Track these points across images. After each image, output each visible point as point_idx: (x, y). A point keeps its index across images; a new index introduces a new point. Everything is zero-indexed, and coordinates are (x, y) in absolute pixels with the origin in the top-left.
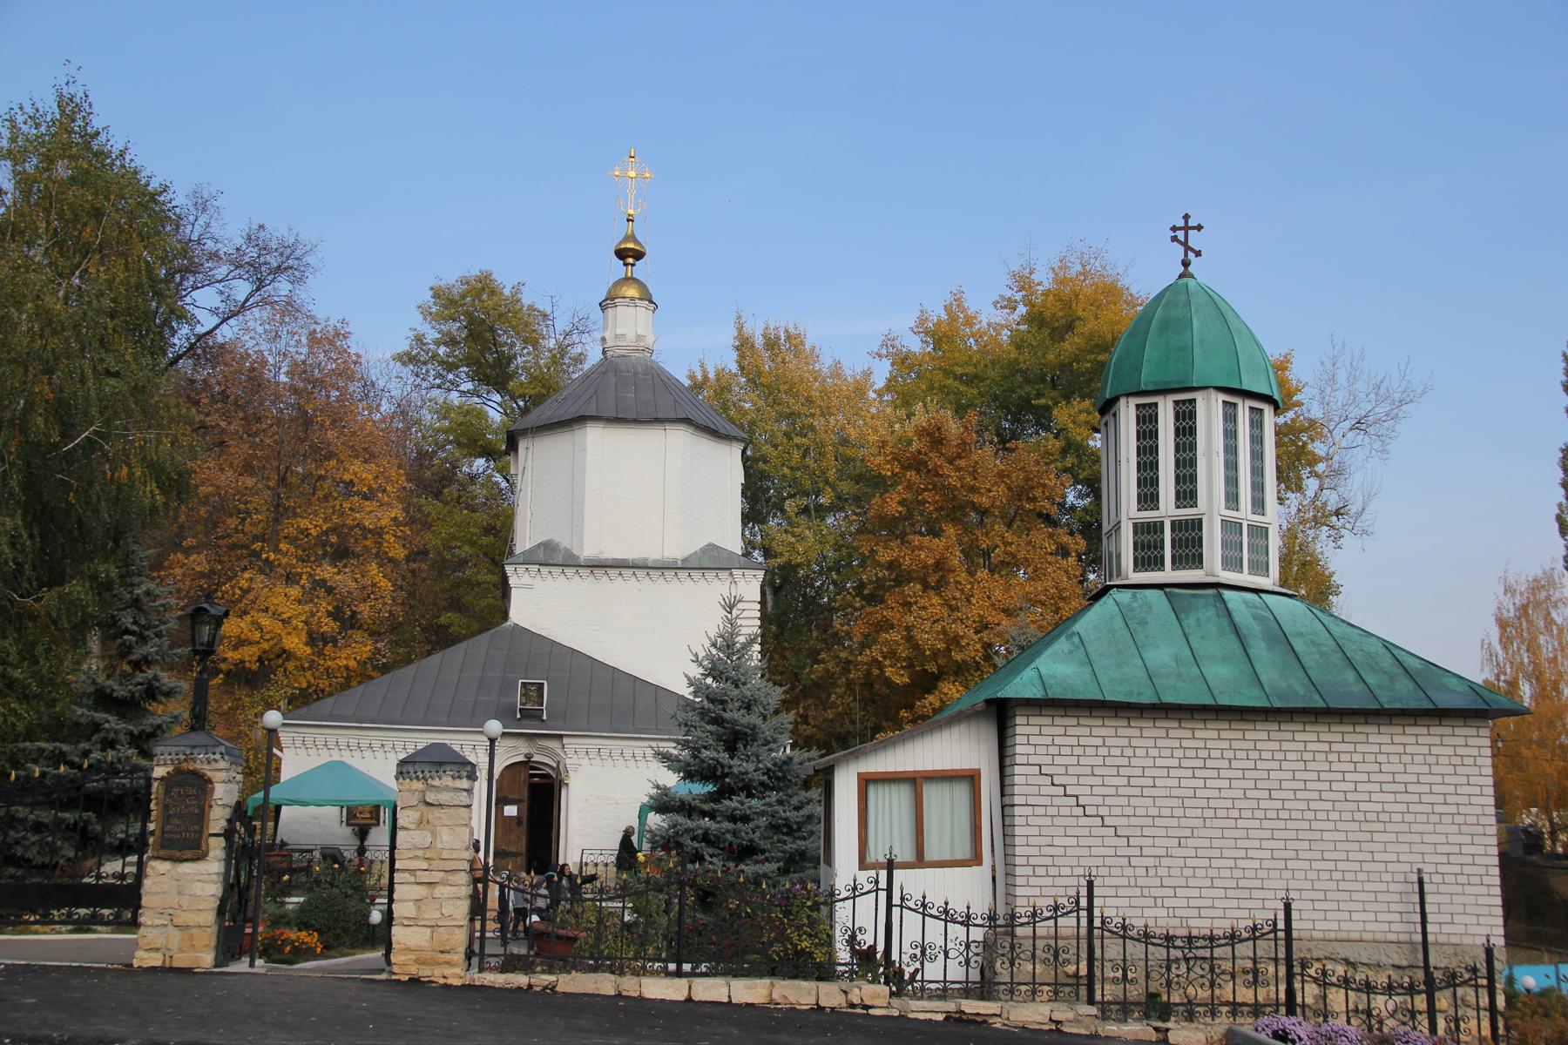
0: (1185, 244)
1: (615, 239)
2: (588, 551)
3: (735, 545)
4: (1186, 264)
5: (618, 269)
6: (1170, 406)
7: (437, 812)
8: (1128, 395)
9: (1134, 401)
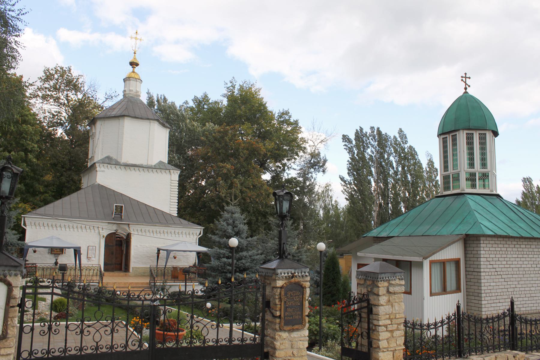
0: (465, 82)
1: (131, 59)
2: (123, 160)
3: (166, 160)
4: (466, 89)
5: (130, 68)
6: (478, 135)
7: (394, 297)
8: (463, 129)
9: (465, 132)
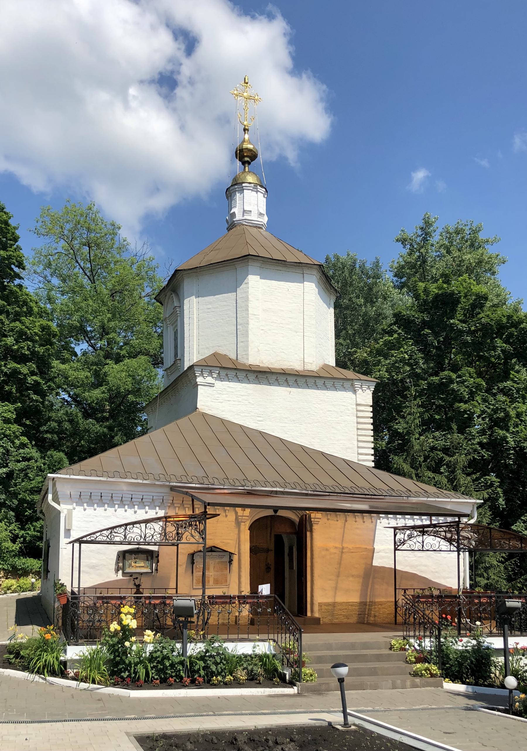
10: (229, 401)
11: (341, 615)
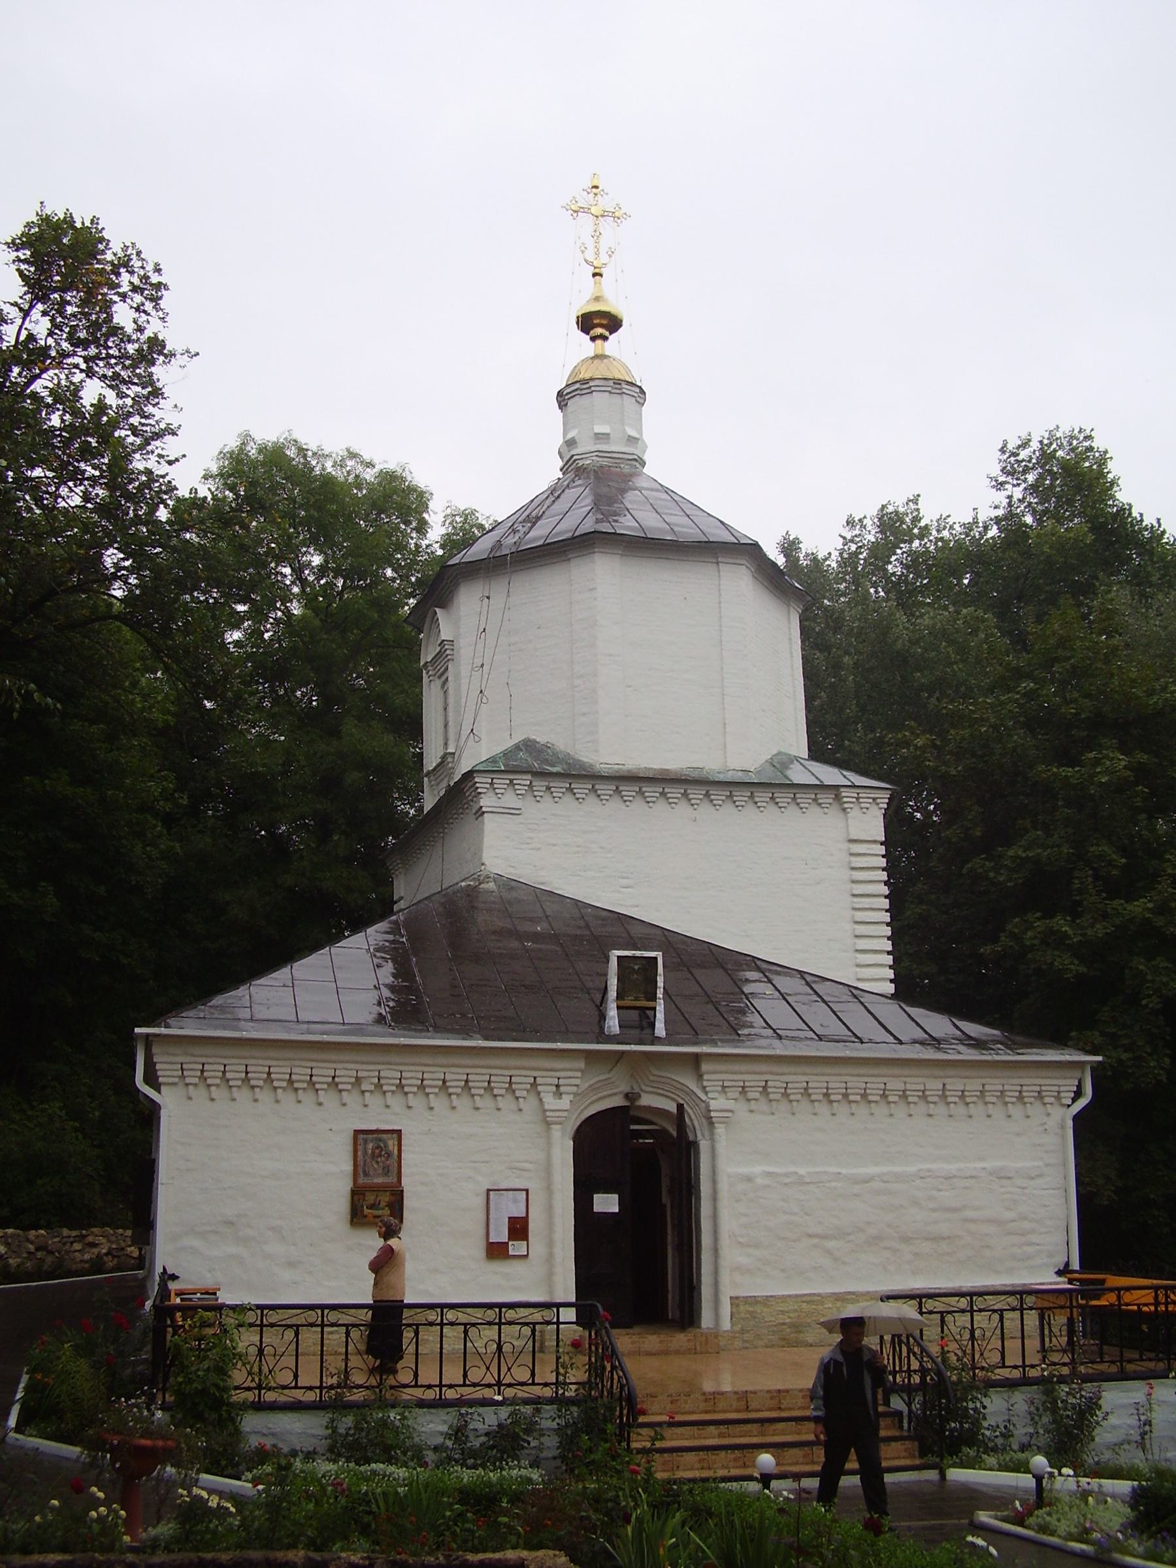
5: (583, 346)
10: (554, 845)
11: (784, 1324)
